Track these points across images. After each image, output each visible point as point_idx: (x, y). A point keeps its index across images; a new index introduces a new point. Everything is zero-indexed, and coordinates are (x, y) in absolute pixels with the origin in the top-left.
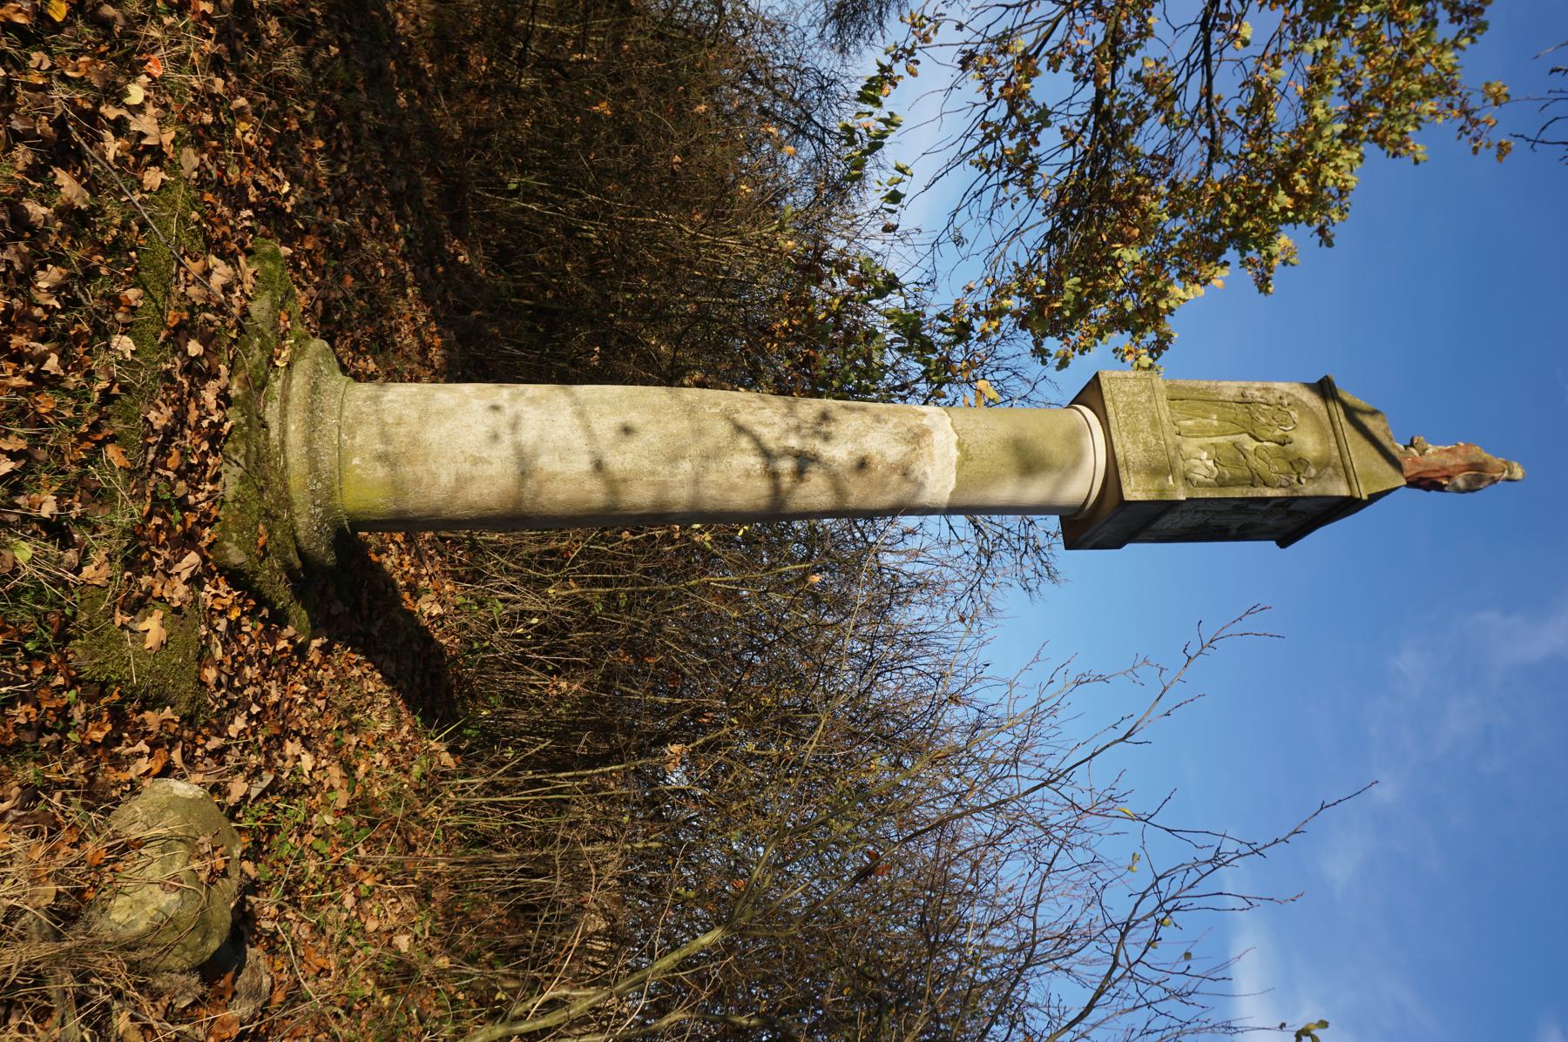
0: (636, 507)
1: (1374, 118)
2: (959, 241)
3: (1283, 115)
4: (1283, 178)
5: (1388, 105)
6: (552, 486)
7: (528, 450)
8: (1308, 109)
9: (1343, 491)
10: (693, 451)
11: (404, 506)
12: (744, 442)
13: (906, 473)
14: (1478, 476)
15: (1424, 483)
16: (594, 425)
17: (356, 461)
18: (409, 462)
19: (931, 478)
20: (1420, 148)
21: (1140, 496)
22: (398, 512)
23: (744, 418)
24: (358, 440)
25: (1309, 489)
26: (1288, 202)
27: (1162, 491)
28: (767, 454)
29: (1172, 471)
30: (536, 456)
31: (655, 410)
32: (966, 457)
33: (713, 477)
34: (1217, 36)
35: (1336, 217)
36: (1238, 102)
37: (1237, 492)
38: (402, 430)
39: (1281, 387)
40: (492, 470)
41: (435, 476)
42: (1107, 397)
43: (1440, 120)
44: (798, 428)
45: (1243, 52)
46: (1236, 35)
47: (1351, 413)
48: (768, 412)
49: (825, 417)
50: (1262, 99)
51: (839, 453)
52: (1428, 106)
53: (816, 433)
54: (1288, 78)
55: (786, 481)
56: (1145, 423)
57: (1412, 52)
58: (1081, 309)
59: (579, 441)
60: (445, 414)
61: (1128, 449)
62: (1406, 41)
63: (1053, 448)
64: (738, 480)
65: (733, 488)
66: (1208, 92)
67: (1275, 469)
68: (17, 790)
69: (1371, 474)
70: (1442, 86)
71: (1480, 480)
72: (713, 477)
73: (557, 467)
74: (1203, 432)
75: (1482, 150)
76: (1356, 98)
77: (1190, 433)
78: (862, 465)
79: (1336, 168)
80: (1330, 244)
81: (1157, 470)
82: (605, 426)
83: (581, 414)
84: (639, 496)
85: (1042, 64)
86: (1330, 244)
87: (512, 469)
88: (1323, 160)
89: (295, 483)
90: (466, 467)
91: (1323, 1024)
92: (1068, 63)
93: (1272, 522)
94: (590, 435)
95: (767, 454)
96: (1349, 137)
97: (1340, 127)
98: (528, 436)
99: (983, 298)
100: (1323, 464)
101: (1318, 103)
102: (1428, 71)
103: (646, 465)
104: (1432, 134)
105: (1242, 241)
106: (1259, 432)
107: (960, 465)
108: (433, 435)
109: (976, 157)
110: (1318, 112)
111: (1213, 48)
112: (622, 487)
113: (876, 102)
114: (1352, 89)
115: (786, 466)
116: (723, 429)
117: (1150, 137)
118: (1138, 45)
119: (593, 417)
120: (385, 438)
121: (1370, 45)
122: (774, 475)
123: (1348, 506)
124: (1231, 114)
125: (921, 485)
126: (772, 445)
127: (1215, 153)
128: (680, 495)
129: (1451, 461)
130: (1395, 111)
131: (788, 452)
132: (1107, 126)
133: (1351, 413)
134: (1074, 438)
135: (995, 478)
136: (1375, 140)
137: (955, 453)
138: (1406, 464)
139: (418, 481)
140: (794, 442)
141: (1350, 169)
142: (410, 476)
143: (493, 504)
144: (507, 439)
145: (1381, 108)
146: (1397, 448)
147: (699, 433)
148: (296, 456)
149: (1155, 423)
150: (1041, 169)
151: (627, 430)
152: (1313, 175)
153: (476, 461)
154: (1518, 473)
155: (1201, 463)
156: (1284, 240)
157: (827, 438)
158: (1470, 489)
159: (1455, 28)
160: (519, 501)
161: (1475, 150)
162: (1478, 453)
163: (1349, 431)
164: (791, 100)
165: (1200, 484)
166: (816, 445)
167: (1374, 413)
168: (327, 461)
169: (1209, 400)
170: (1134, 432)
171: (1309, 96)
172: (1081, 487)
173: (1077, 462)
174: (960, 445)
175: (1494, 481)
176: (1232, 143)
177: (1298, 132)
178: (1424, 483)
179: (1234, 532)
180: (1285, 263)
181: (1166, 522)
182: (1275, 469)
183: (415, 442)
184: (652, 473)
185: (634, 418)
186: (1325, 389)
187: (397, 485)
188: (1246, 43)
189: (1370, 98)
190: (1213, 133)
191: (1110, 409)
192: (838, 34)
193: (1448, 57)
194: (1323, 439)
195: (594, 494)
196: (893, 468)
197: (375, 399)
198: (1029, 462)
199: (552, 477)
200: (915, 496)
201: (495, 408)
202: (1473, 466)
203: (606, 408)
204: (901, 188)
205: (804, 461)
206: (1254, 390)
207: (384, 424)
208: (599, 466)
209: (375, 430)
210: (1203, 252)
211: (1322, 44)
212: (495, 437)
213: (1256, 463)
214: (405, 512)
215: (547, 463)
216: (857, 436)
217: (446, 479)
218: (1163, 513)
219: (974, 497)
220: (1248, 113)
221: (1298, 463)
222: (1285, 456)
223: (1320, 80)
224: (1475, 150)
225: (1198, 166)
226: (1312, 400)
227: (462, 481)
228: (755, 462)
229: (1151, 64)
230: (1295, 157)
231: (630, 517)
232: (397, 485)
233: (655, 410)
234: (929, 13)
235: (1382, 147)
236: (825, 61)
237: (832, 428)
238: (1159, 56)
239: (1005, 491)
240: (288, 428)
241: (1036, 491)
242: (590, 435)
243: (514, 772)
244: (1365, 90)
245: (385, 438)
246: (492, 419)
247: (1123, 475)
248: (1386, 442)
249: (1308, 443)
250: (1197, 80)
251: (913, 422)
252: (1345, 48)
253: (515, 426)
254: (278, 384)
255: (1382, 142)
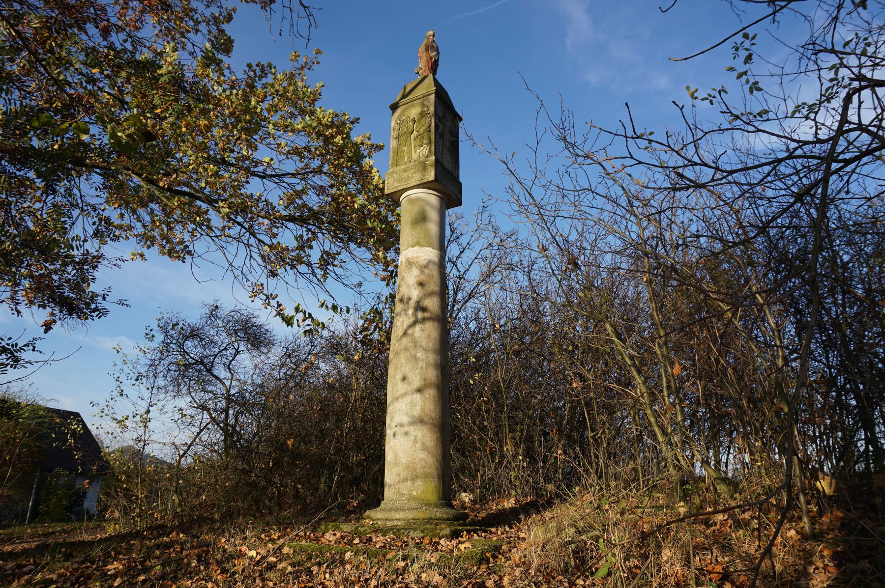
0: (437, 376)
1: (302, 103)
2: (360, 285)
3: (301, 141)
4: (327, 140)
5: (299, 99)
6: (427, 411)
7: (411, 420)
8: (299, 131)
9: (433, 96)
10: (413, 351)
11: (435, 475)
12: (410, 332)
13: (426, 267)
14: (432, 47)
15: (434, 67)
16: (401, 393)
17: (415, 493)
18: (415, 470)
19: (426, 257)
20: (318, 85)
21: (433, 173)
22: (438, 478)
23: (400, 333)
24: (406, 492)
25: (432, 109)
26: (339, 137)
27: (431, 165)
28: (415, 323)
29: (424, 162)
30: (414, 416)
31: (396, 369)
32: (418, 244)
33: (424, 344)
34: (269, 172)
35: (347, 117)
36: (298, 162)
37: (433, 136)
38: (402, 473)
39: (393, 124)
40: (420, 435)
41: (422, 460)
42: (395, 190)
43: (305, 78)
44: (405, 311)
45: (276, 160)
46: (268, 163)
47: (404, 97)
48: (398, 324)
49: (401, 300)
50: (297, 152)
51: (415, 294)
52: (300, 84)
53: (407, 303)
54: (287, 140)
55: (427, 315)
56: (405, 174)
57: (277, 91)
58: (384, 220)
59: (408, 399)
60: (396, 456)
61: (416, 179)
62: (273, 94)
63: (415, 209)
64: (426, 334)
65: (429, 336)
66: (294, 175)
67: (425, 122)
68: (160, 41)
69: (428, 86)
70: (291, 77)
71: (433, 46)
72: (424, 344)
73: (418, 408)
74: (410, 152)
75: (318, 60)
76: (296, 113)
77: (410, 157)
78: (421, 284)
79: (324, 118)
80: (359, 119)
81: (424, 167)
82: (401, 388)
83: (397, 399)
84: (432, 374)
85: (275, 241)
86: (359, 119)
87: (419, 426)
88: (320, 123)
89: (422, 516)
90: (418, 445)
91: (688, 88)
92: (275, 230)
93: (449, 124)
94: (405, 394)
95: (415, 323)
96: (312, 113)
97: (307, 118)
98: (405, 420)
99: (380, 267)
100: (423, 105)
101: (296, 126)
102: (285, 84)
103: (418, 371)
104: (311, 81)
105: (358, 158)
106: (410, 131)
107: (421, 246)
108: (404, 460)
109: (322, 280)
110: (300, 127)
111: (274, 173)
112: (428, 381)
113: (292, 318)
114: (293, 115)
115: (420, 315)
116: (405, 341)
117: (313, 200)
118: (271, 205)
119: (398, 394)
120: (406, 480)
121: (274, 108)
122: (424, 320)
123: (441, 96)
124: (303, 164)
125: (430, 262)
126: (411, 320)
127: (319, 171)
128: (432, 358)
129: (424, 58)
130: (301, 96)
131: (415, 314)
132: (305, 218)
133: (404, 97)
134: (412, 201)
135: (427, 233)
136: (313, 103)
137: (416, 248)
138: (425, 74)
139: (424, 467)
140: (410, 312)
141: (325, 110)
142: (422, 470)
143: (435, 436)
144: (406, 429)
145: (300, 102)
146: (419, 78)
147: (406, 349)
148: (410, 515)
149: (405, 170)
150: (327, 249)
151: (404, 379)
152: (328, 127)
153: (415, 441)
154: (431, 33)
155: (422, 151)
156: (356, 138)
157: (409, 299)
158: (437, 50)
159: (269, 75)
160: (434, 425)
161: (318, 63)
162: (422, 48)
163: (411, 96)
164: (295, 370)
165: (430, 151)
166: (412, 303)
167: (405, 88)
168: (414, 504)
169: (398, 151)
170: (408, 178)
171: (293, 131)
172: (431, 198)
173: (418, 199)
174: (413, 246)
175: (434, 41)
176: (316, 163)
177: (309, 134)
178: (434, 67)
179: (454, 139)
180: (369, 139)
181: (448, 164)
182: (425, 122)
183: (407, 467)
184: (422, 369)
185: (399, 376)
186: (394, 107)
187: (426, 476)
188: (272, 159)
189: (296, 107)
190: (311, 172)
191: (400, 188)
192: (265, 346)
193: (279, 77)
194: (414, 106)
195: (431, 393)
196: (422, 272)
197: (390, 486)
198: (421, 218)
199: (423, 410)
200: (434, 263)
201: (394, 435)
202: (427, 50)
203: (395, 389)
204: (330, 306)
205: (420, 307)
206: (394, 134)
207: (399, 482)
208: (419, 390)
209: (402, 485)
210: (363, 176)
211: (271, 126)
212: (406, 434)
213: (422, 130)
214: (438, 475)
215: (417, 411)
216: (408, 287)
217: (423, 455)
218: (443, 166)
219: (435, 241)
220: (302, 157)
221: (423, 115)
222: (420, 120)
223: (287, 127)
224: (318, 63)
225: (324, 177)
226: (399, 111)
227: (424, 448)
228: (418, 328)
229: (281, 202)
230: (319, 134)
231: (442, 380)
232: (426, 476)
233: (396, 369)
234: (251, 289)
235: (316, 100)
236: (275, 354)
237: (405, 297)
238: (278, 198)
239: (433, 227)
240: (399, 517)
241: (434, 215)
242: (405, 394)
243: (590, 463)
244: (292, 110)
245: (406, 480)
246: (398, 436)
247: (425, 181)
248: (416, 83)
249: (414, 112)
250: (287, 179)
251: (404, 265)
252: (276, 118)
253: (402, 425)
254: (379, 523)
255: (314, 101)
